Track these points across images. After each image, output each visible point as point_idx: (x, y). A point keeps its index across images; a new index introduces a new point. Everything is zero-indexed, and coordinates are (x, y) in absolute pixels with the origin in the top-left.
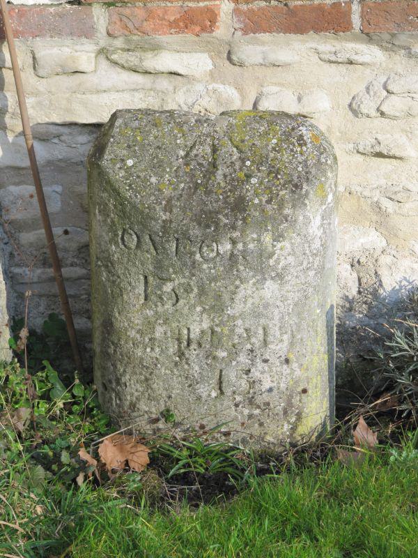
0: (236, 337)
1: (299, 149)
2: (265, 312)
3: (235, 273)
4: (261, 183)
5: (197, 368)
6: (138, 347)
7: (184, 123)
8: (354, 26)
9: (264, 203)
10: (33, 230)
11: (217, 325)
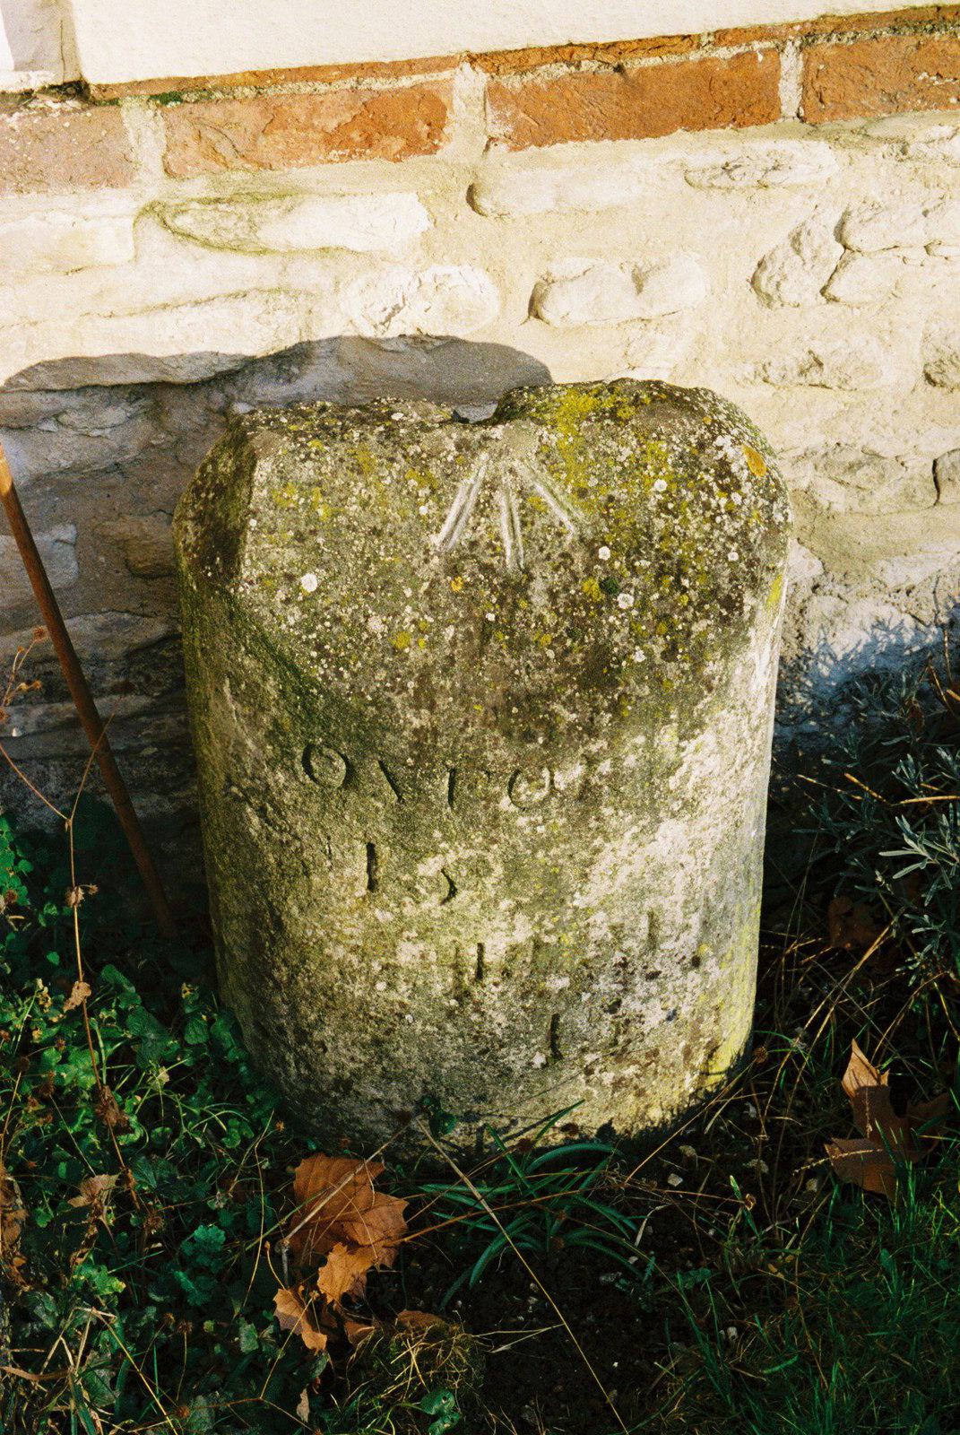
0: (592, 946)
1: (723, 502)
2: (654, 885)
3: (593, 824)
4: (643, 606)
5: (501, 1018)
6: (354, 979)
7: (430, 456)
8: (783, 108)
9: (658, 660)
10: (16, 629)
11: (547, 933)
